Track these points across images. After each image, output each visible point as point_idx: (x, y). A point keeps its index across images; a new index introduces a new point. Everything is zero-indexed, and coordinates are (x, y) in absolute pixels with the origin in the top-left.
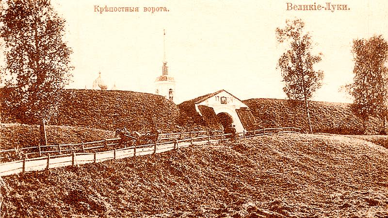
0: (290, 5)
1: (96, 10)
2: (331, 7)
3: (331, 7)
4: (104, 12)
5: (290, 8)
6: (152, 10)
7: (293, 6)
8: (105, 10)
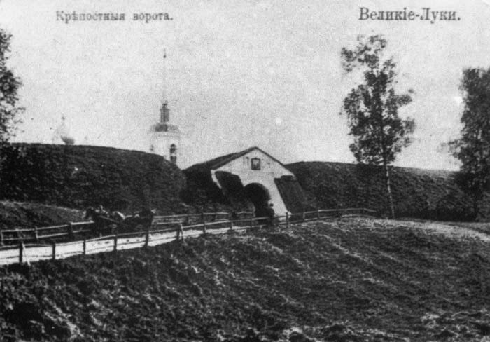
0: (365, 11)
1: (59, 18)
2: (431, 17)
3: (431, 17)
4: (71, 21)
5: (364, 16)
6: (407, 14)
7: (369, 14)
8: (72, 17)
